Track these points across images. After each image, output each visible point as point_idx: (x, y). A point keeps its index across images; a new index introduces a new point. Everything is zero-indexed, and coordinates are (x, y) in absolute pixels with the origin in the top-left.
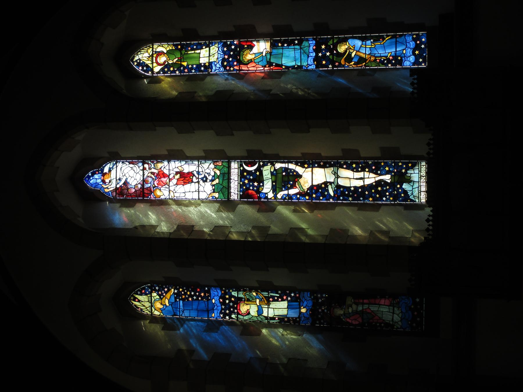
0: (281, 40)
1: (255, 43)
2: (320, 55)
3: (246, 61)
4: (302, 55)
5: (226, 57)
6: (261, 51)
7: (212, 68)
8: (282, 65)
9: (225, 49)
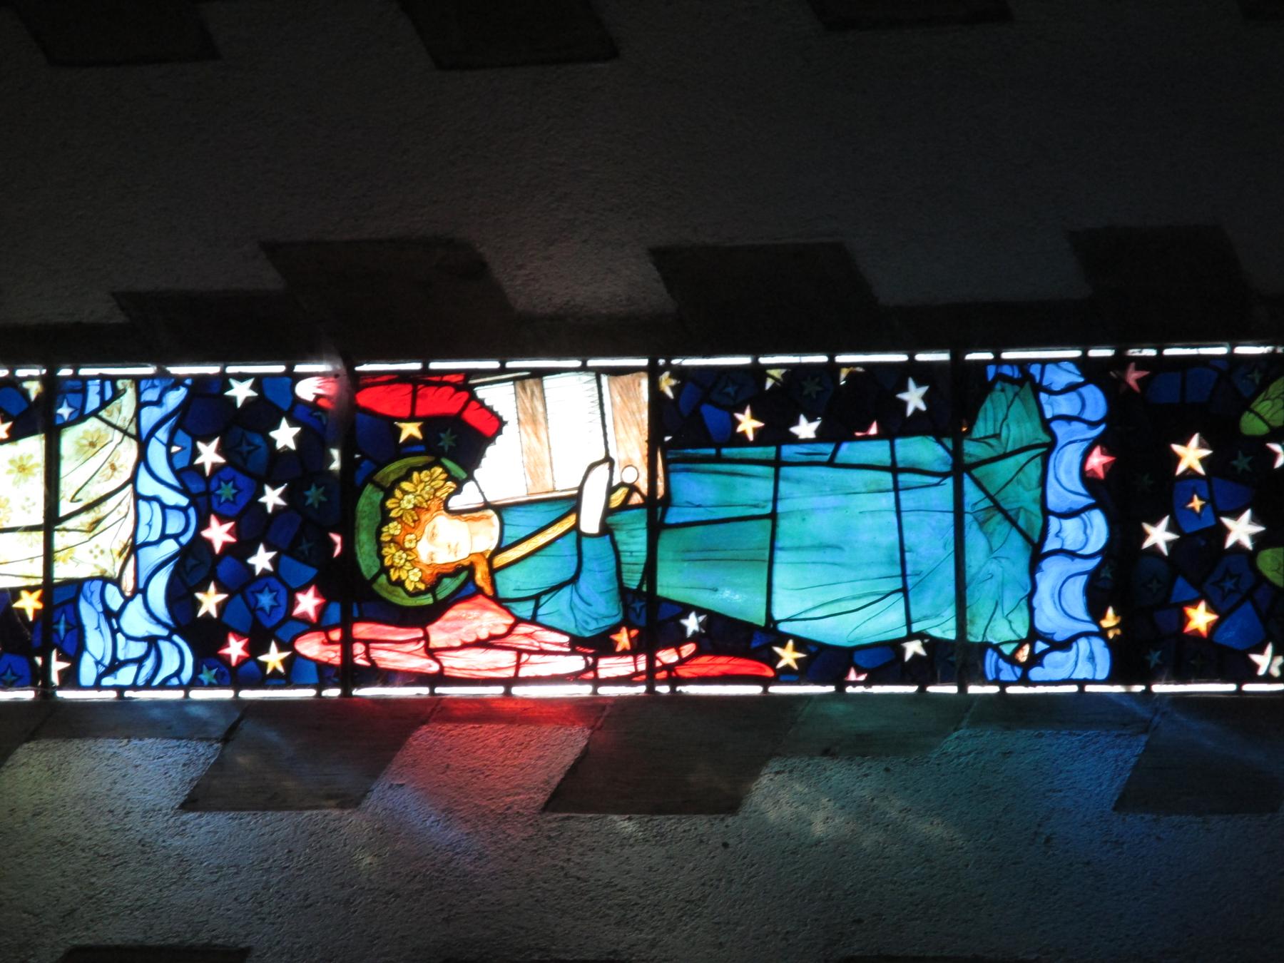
0: (759, 372)
1: (498, 396)
2: (1159, 535)
3: (413, 579)
4: (976, 542)
5: (218, 534)
6: (565, 483)
7: (75, 649)
8: (771, 634)
9: (209, 455)
